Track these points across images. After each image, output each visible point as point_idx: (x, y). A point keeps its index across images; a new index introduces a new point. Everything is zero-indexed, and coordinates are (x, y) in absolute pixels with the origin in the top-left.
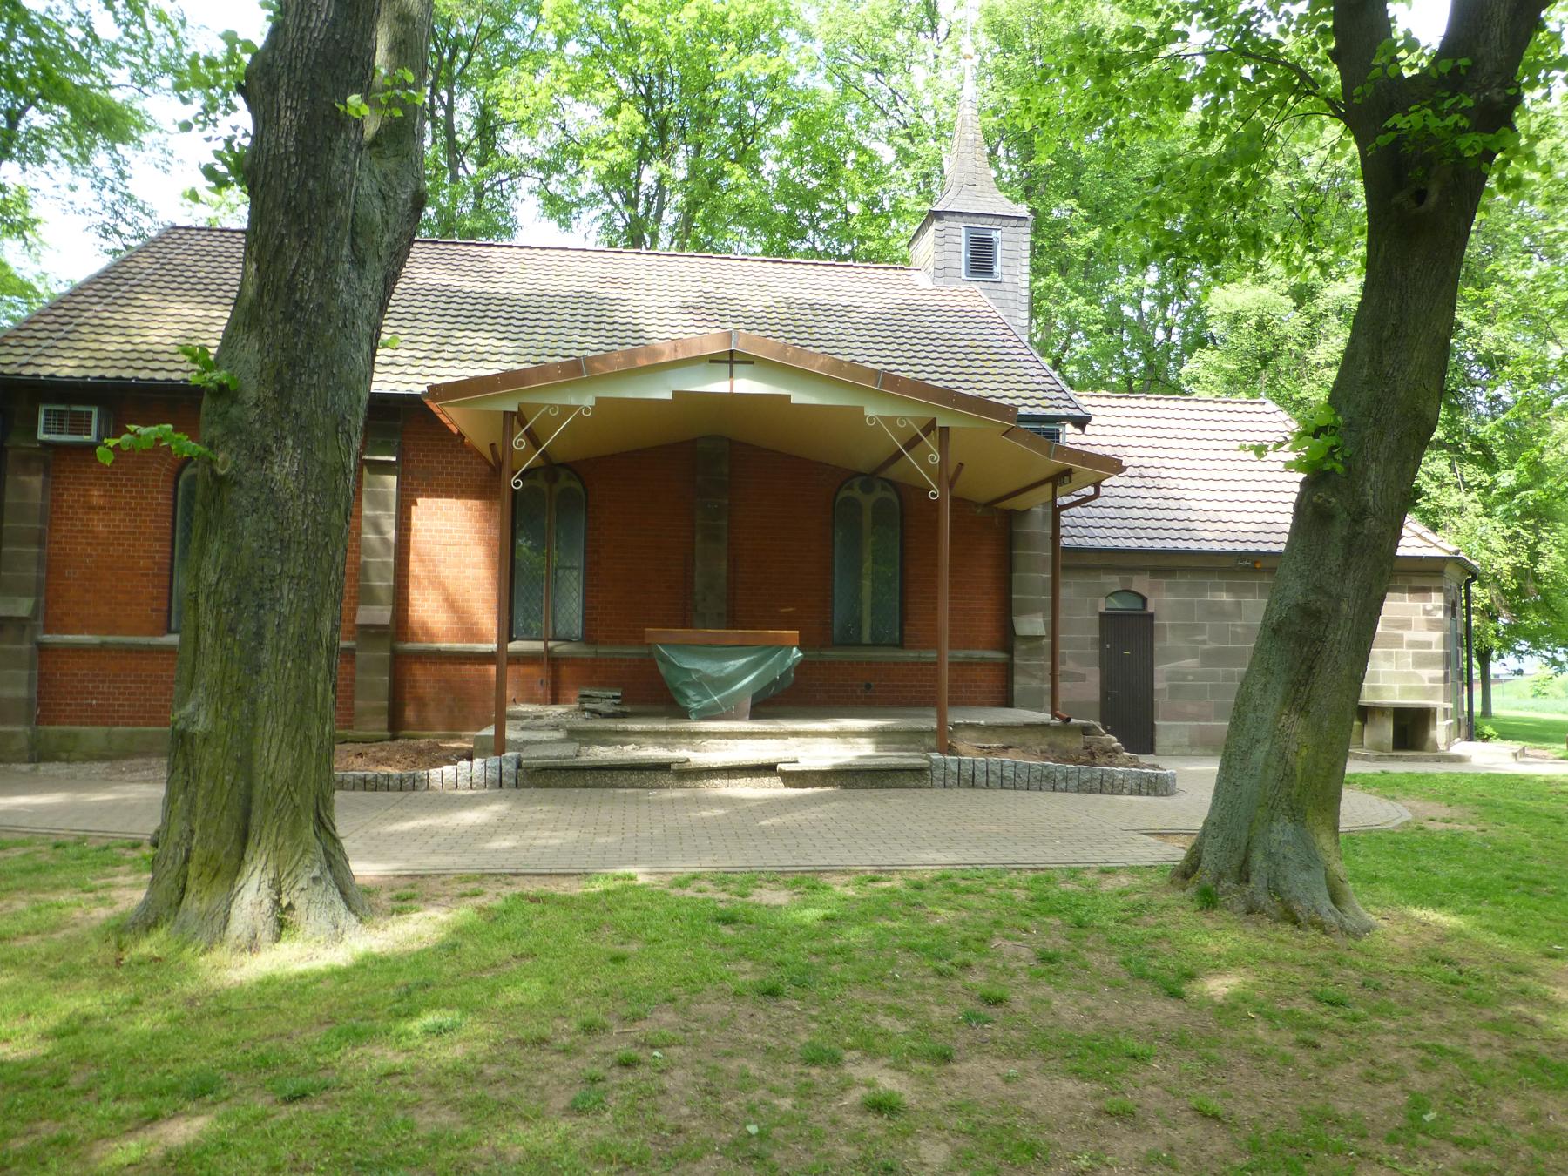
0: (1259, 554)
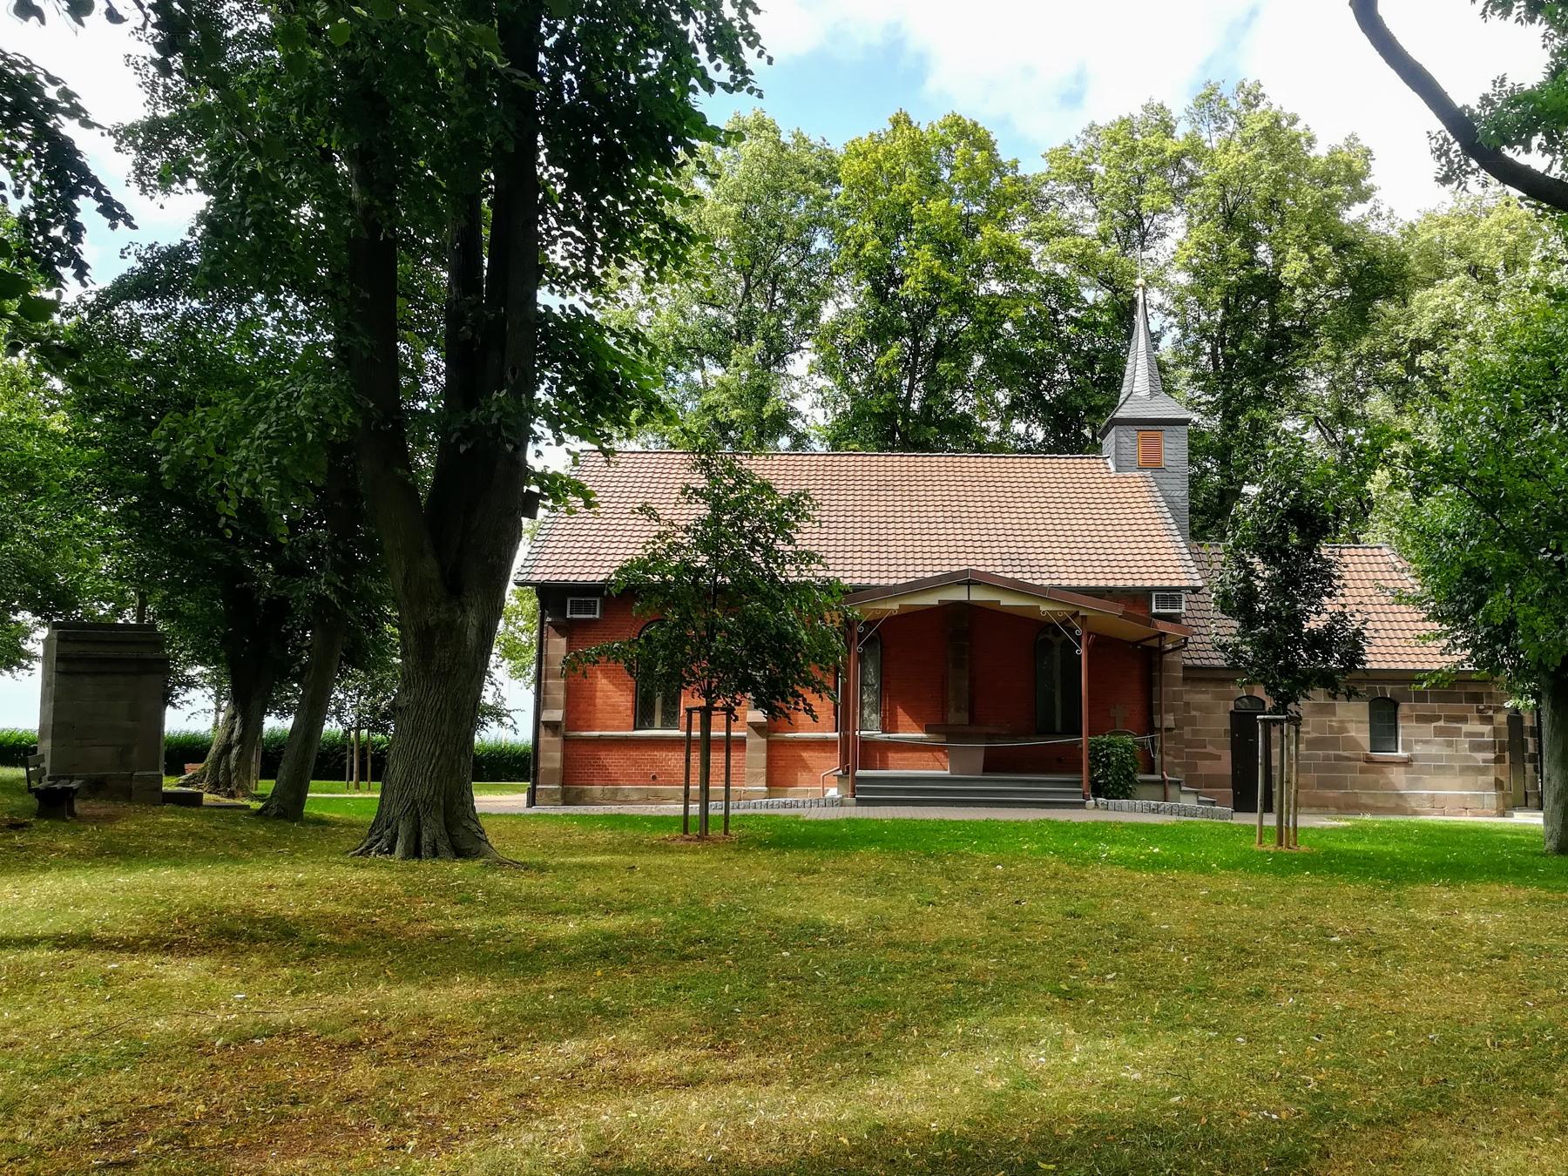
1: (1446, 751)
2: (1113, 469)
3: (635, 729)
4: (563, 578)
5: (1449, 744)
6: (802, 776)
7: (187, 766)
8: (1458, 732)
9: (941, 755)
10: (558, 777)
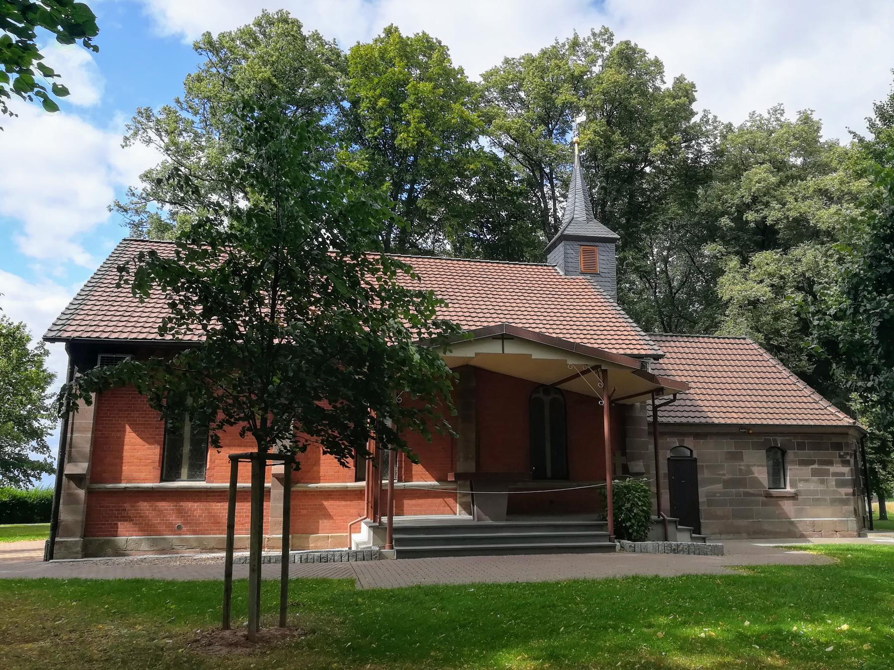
0: (750, 425)
1: (821, 487)
2: (562, 273)
3: (162, 480)
4: (95, 335)
5: (822, 482)
6: (324, 523)
7: (417, 468)
8: (827, 473)
9: (450, 501)
10: (79, 530)
